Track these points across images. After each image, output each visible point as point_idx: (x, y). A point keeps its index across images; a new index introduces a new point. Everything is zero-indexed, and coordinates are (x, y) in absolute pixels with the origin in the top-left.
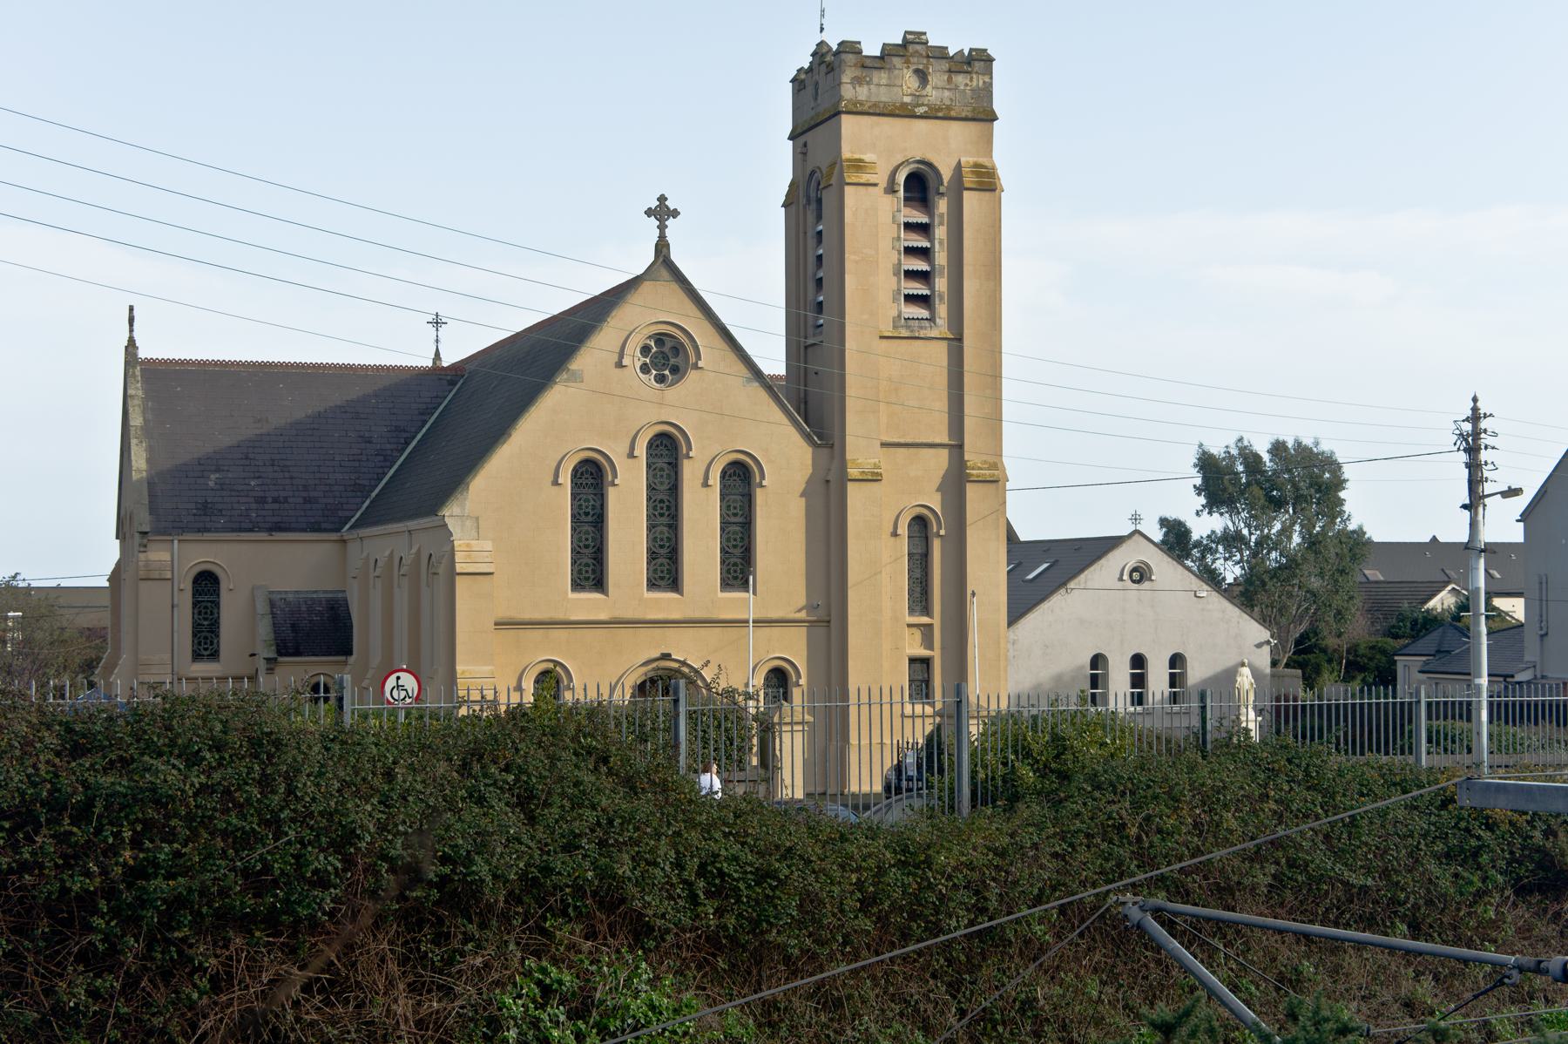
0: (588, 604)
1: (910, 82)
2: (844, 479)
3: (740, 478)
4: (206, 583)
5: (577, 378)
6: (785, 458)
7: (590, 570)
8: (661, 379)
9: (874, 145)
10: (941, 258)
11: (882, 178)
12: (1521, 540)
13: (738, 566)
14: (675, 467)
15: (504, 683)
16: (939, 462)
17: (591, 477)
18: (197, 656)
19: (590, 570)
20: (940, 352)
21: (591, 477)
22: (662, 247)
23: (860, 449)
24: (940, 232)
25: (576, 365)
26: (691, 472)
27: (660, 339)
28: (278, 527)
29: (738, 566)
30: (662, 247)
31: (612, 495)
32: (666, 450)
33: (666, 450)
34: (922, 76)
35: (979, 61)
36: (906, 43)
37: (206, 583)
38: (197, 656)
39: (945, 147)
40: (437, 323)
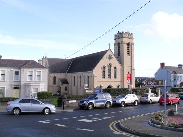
0: (104, 80)
1: (128, 35)
2: (124, 69)
3: (115, 68)
4: (55, 78)
5: (103, 59)
6: (119, 67)
7: (104, 77)
8: (109, 59)
9: (125, 40)
10: (130, 50)
11: (126, 43)
12: (154, 77)
13: (115, 77)
14: (110, 67)
15: (115, 86)
16: (130, 68)
17: (104, 68)
18: (54, 84)
19: (104, 77)
20: (130, 58)
21: (104, 68)
22: (109, 48)
23: (125, 67)
24: (130, 48)
25: (103, 58)
26: (112, 68)
27: (109, 56)
28: (60, 73)
29: (115, 77)
30: (109, 48)
31: (106, 70)
32: (110, 66)
33: (110, 66)
34: (128, 35)
35: (132, 34)
36: (127, 32)
37: (55, 78)
38: (54, 84)
39: (130, 41)
40: (65, 56)
